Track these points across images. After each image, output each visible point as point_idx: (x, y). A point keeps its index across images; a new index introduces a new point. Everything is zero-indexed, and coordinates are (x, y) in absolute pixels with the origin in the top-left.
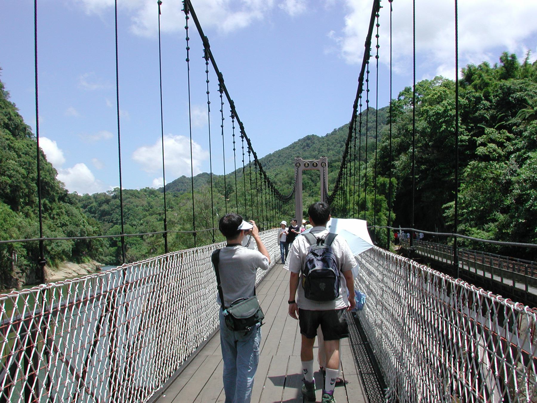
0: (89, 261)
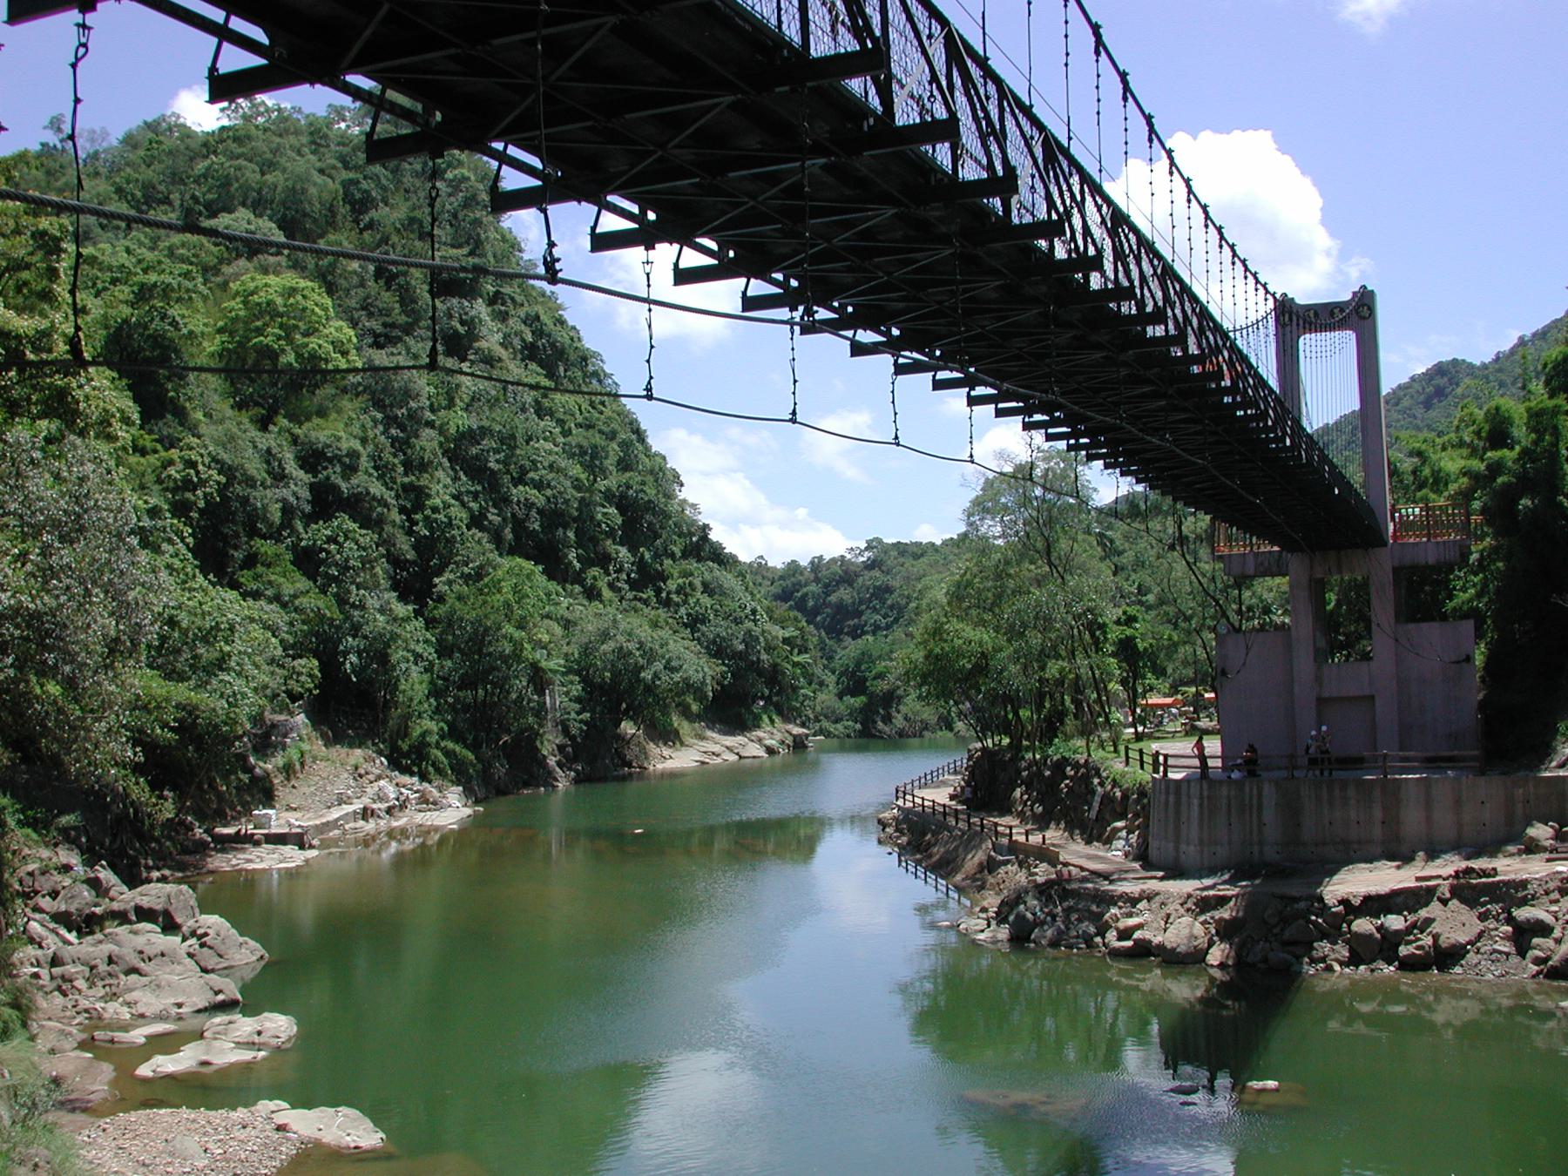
0: (772, 721)
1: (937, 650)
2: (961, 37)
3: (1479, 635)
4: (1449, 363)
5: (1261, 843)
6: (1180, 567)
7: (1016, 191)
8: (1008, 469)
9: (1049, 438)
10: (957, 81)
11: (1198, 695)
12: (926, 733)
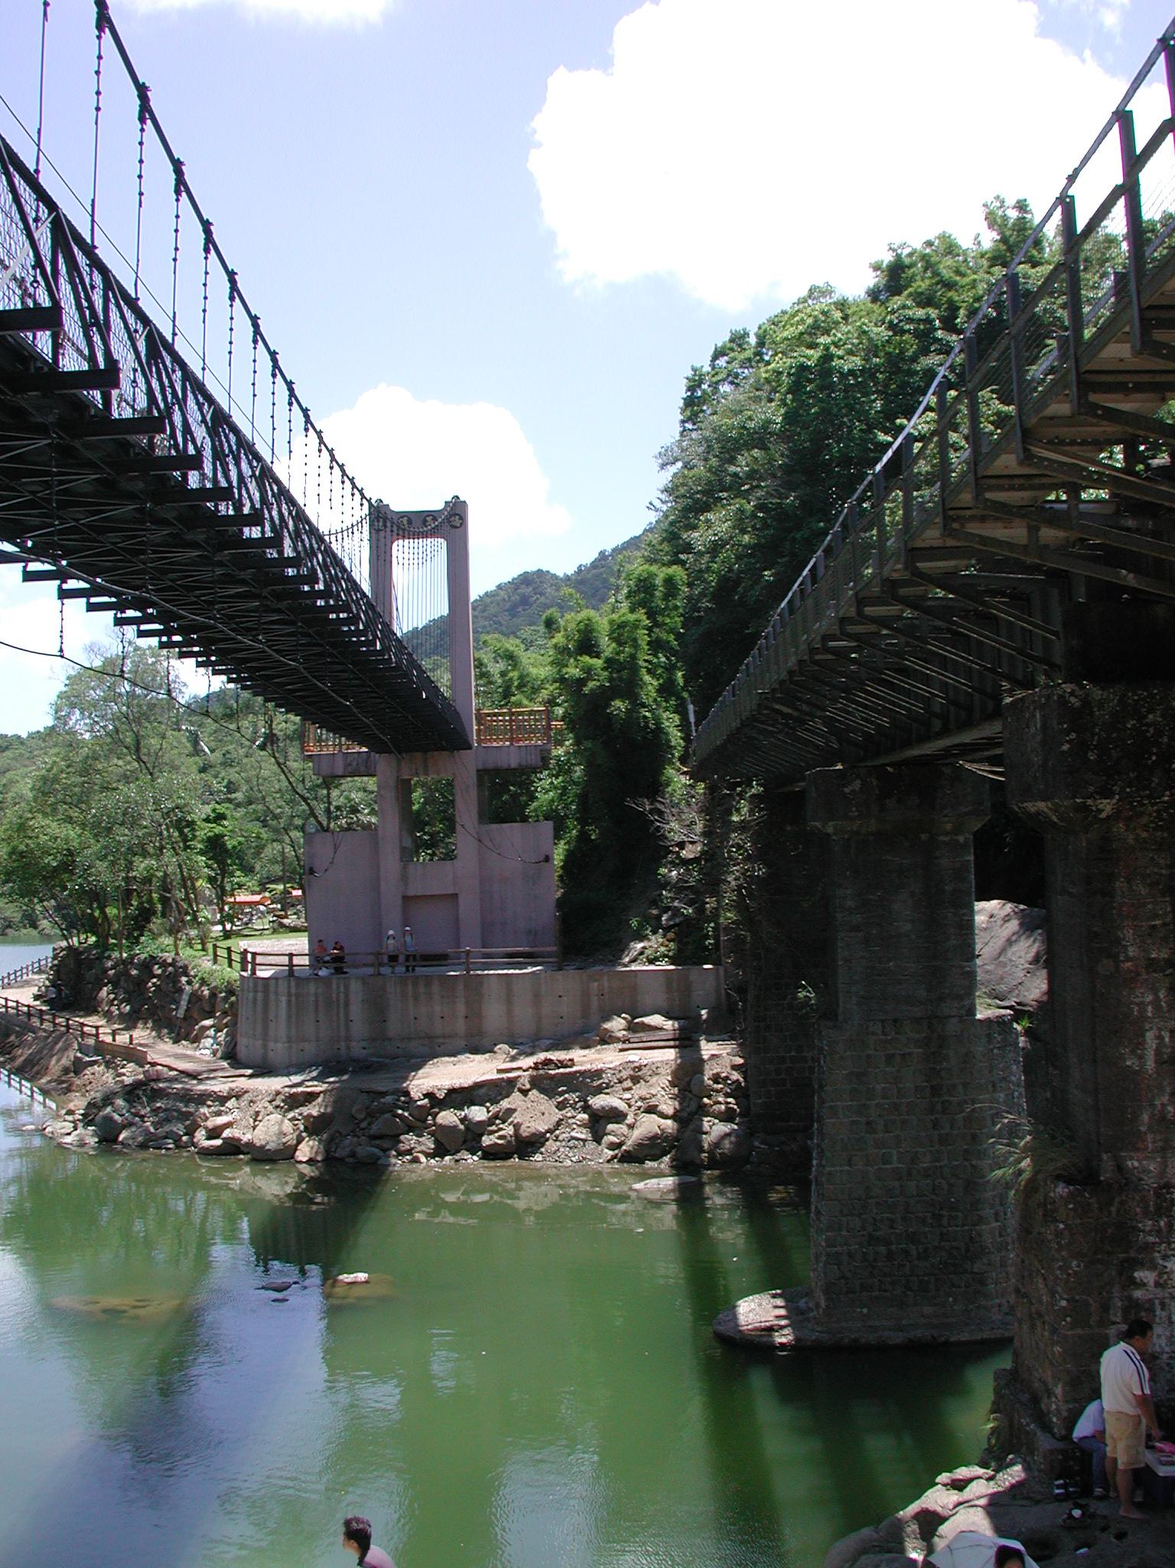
1: (22, 847)
2: (68, 222)
3: (558, 833)
4: (534, 573)
5: (348, 1039)
6: (269, 768)
7: (117, 385)
8: (97, 663)
9: (142, 634)
10: (63, 268)
11: (286, 892)
12: (9, 931)
